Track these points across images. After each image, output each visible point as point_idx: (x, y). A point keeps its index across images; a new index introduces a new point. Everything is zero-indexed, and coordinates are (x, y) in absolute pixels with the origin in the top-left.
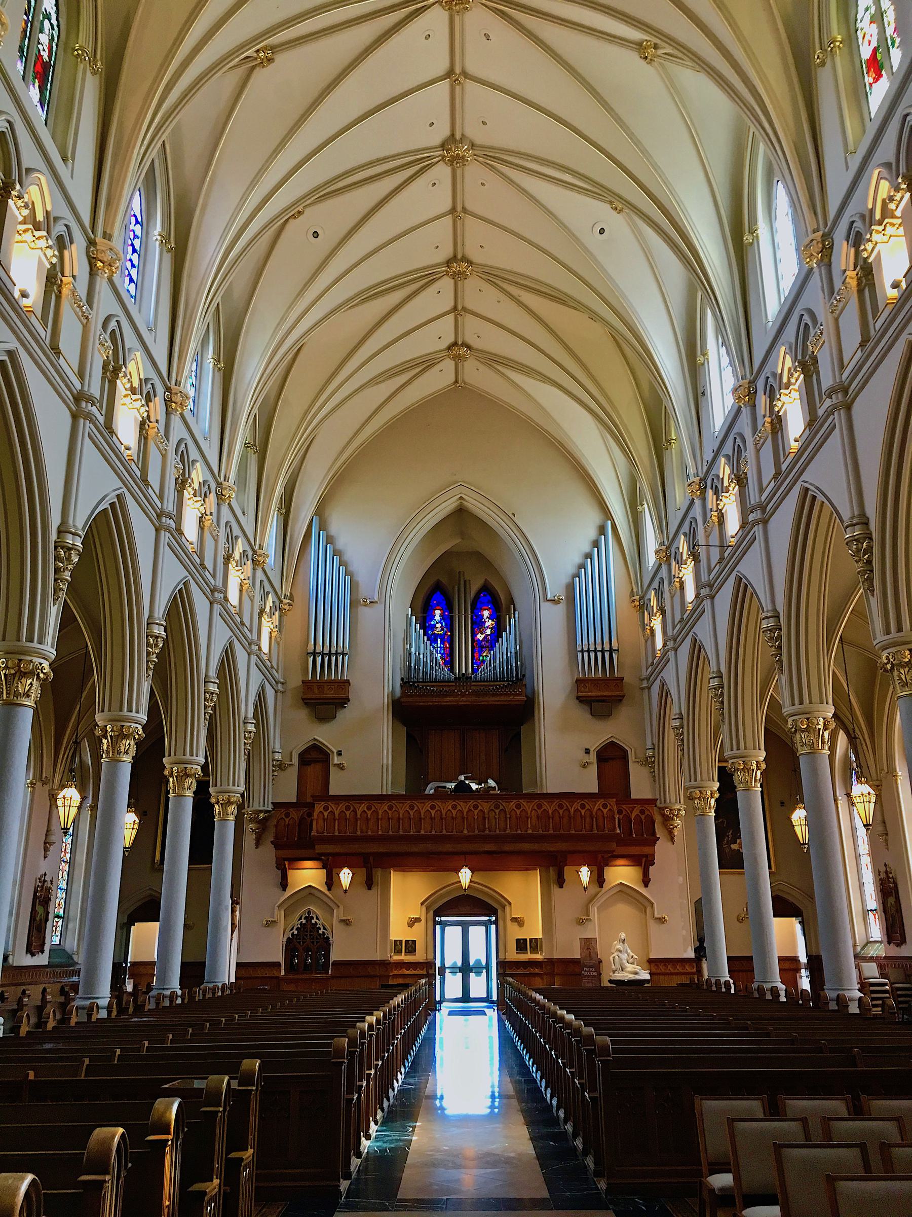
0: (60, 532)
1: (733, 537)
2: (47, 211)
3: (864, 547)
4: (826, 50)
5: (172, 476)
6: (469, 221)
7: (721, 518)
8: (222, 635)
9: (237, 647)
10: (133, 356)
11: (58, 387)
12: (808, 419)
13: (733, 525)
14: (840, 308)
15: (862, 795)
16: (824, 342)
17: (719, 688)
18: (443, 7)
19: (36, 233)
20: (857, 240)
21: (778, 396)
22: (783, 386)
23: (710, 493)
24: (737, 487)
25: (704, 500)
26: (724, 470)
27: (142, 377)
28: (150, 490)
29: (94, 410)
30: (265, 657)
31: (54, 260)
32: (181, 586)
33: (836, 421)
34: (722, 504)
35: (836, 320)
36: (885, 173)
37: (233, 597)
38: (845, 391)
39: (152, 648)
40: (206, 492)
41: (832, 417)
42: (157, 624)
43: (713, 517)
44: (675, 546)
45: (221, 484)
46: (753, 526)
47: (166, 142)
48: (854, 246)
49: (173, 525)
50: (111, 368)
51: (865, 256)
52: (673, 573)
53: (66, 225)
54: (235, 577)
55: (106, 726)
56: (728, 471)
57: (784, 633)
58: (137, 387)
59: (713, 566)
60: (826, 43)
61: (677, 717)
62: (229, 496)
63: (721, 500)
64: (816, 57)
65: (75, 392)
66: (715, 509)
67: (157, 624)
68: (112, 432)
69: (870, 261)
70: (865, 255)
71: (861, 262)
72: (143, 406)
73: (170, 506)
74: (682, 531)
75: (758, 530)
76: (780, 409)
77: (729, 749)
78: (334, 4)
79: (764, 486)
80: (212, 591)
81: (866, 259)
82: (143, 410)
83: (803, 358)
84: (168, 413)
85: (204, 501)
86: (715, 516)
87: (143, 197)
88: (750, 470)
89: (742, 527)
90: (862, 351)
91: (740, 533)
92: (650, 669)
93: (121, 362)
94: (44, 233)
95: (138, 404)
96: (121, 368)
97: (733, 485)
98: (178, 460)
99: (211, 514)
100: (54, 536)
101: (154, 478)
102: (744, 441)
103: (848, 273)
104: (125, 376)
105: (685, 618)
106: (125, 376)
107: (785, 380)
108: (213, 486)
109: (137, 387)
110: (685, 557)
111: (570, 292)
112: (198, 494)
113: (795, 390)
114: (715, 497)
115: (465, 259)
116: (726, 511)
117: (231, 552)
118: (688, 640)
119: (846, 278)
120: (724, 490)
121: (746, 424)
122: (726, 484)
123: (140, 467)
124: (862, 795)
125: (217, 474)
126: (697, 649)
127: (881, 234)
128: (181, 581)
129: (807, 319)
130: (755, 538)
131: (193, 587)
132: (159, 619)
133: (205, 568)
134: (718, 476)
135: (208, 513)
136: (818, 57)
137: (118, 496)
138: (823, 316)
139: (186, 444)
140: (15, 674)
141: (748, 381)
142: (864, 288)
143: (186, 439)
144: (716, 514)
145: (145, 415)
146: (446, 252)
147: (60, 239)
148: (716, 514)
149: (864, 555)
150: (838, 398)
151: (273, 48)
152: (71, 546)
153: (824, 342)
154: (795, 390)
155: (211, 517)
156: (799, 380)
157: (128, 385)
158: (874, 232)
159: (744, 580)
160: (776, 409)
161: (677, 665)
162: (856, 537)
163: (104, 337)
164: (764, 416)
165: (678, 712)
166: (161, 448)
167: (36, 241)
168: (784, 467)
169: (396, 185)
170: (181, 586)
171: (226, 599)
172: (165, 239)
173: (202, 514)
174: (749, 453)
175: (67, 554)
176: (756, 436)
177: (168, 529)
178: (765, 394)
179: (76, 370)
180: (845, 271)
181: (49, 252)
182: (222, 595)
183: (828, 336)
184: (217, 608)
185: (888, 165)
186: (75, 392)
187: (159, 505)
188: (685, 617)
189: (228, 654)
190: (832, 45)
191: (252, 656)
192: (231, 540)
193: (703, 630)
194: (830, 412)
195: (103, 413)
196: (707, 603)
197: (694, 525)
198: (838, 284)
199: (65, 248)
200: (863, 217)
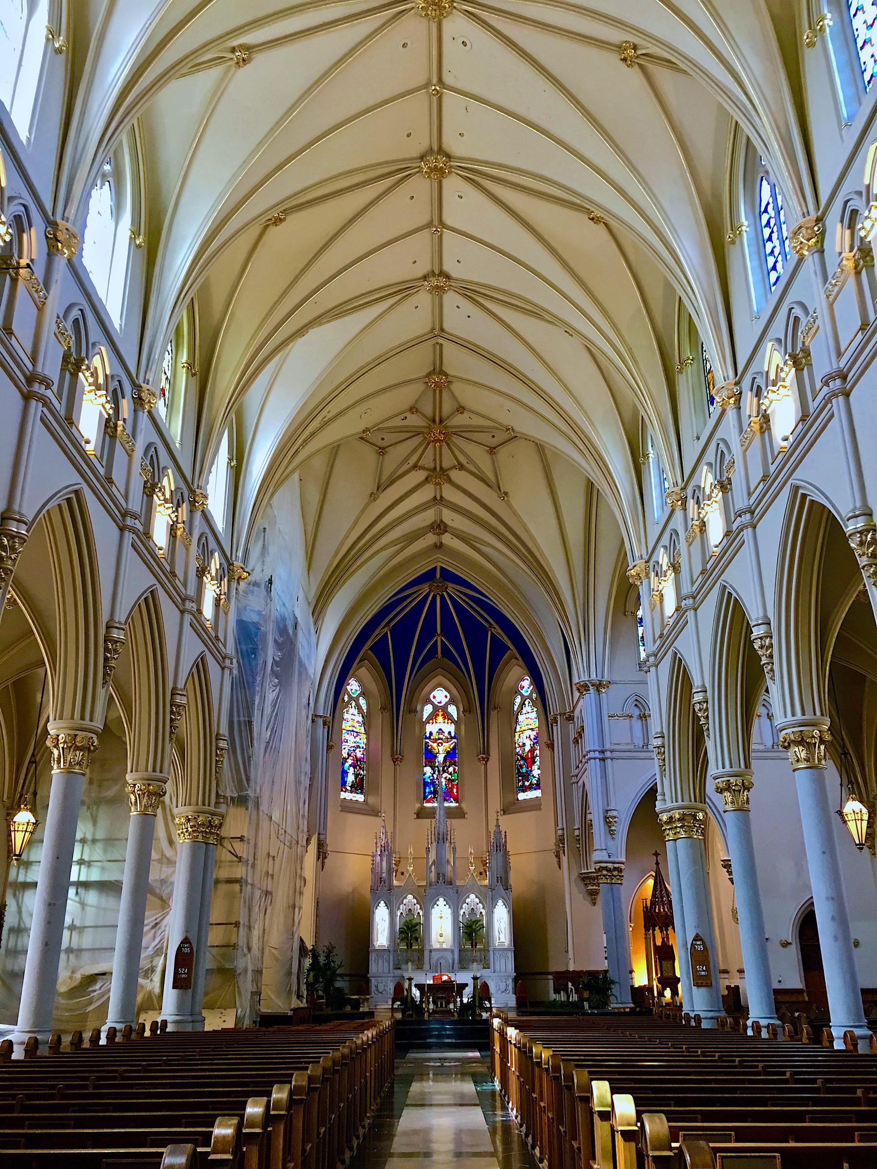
0: (108, 627)
1: (716, 547)
2: (106, 375)
3: (869, 539)
4: (815, 30)
5: (194, 565)
6: (447, 234)
7: (703, 525)
8: (193, 648)
9: (210, 659)
10: (97, 350)
11: (61, 441)
12: (801, 414)
13: (716, 533)
14: (834, 293)
15: (854, 812)
16: (818, 328)
17: (704, 702)
18: (424, 177)
19: (165, 505)
20: (852, 219)
21: (765, 394)
22: (770, 383)
23: (691, 503)
24: (794, 369)
25: (685, 509)
26: (663, 558)
27: (108, 372)
28: (13, 340)
29: (49, 393)
30: (208, 624)
31: (111, 412)
32: (148, 594)
33: (835, 409)
34: (703, 512)
35: (831, 306)
36: (776, 346)
37: (160, 537)
38: (844, 378)
39: (175, 716)
40: (178, 500)
41: (830, 405)
42: (117, 628)
43: (694, 527)
44: (654, 559)
45: (56, 224)
46: (686, 611)
47: (194, 298)
48: (756, 396)
49: (141, 528)
50: (72, 360)
51: (863, 235)
52: (652, 587)
53: (81, 310)
54: (210, 591)
55: (58, 736)
56: (666, 560)
57: (775, 641)
58: (102, 383)
59: (695, 578)
60: (815, 21)
61: (760, 622)
62: (203, 503)
63: (703, 508)
64: (805, 37)
65: (28, 373)
66: (696, 518)
67: (117, 628)
68: (72, 423)
69: (868, 240)
70: (862, 233)
71: (857, 243)
72: (173, 512)
73: (135, 504)
74: (662, 543)
75: (747, 533)
76: (768, 408)
77: (670, 801)
78: (311, 3)
79: (843, 350)
80: (183, 600)
81: (862, 239)
82: (173, 516)
83: (793, 350)
84: (50, 256)
85: (220, 585)
86: (696, 525)
87: (113, 189)
88: (683, 561)
89: (727, 534)
90: (862, 334)
91: (725, 541)
92: (658, 642)
93: (83, 354)
94: (104, 392)
95: (170, 511)
96: (83, 360)
97: (716, 491)
98: (200, 552)
99: (183, 522)
100: (102, 631)
101: (118, 476)
102: (677, 535)
103: (843, 255)
104: (88, 369)
105: (665, 633)
106: (88, 369)
107: (772, 376)
108: (186, 493)
109: (102, 383)
110: (665, 568)
111: (545, 305)
112: (214, 579)
113: (716, 502)
114: (696, 506)
115: (443, 274)
116: (708, 520)
117: (206, 564)
118: (670, 654)
119: (842, 260)
120: (663, 575)
121: (732, 426)
122: (708, 491)
123: (169, 561)
124: (854, 812)
125: (134, 376)
126: (679, 665)
127: (776, 394)
128: (149, 588)
129: (798, 311)
130: (744, 542)
131: (162, 596)
132: (120, 623)
133: (175, 576)
134: (699, 487)
135: (180, 521)
136: (729, 237)
137: (152, 592)
138: (818, 302)
139: (155, 448)
140: (71, 747)
141: (680, 488)
142: (764, 432)
143: (155, 443)
144: (697, 523)
145: (175, 519)
146: (421, 142)
147: (18, 218)
148: (697, 523)
149: (868, 548)
150: (837, 384)
151: (248, 48)
152: (15, 534)
153: (818, 328)
154: (716, 502)
155: (182, 525)
156: (790, 374)
157: (162, 498)
158: (873, 208)
159: (679, 655)
160: (763, 407)
161: (657, 676)
162: (859, 530)
163: (64, 325)
164: (750, 416)
165: (659, 730)
166: (128, 448)
167: (98, 398)
168: (772, 468)
169: (358, 39)
170: (148, 594)
171: (200, 611)
172: (190, 366)
173: (173, 522)
174: (682, 546)
175: (11, 542)
176: (827, 285)
177: (133, 530)
178: (842, 221)
179: (29, 352)
180: (840, 253)
181: (108, 406)
182: (194, 605)
183: (823, 322)
184: (188, 617)
185: (779, 340)
186: (123, 511)
187: (184, 591)
188: (665, 633)
189: (200, 666)
190: (821, 24)
191: (127, 533)
192: (206, 554)
193: (686, 645)
194: (828, 400)
195: (104, 464)
196: (690, 614)
197: (674, 537)
198: (745, 427)
199: (23, 232)
200: (860, 193)
